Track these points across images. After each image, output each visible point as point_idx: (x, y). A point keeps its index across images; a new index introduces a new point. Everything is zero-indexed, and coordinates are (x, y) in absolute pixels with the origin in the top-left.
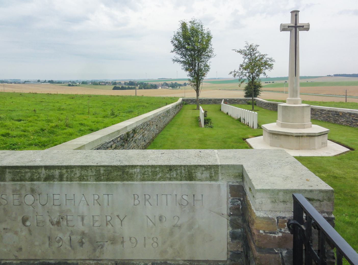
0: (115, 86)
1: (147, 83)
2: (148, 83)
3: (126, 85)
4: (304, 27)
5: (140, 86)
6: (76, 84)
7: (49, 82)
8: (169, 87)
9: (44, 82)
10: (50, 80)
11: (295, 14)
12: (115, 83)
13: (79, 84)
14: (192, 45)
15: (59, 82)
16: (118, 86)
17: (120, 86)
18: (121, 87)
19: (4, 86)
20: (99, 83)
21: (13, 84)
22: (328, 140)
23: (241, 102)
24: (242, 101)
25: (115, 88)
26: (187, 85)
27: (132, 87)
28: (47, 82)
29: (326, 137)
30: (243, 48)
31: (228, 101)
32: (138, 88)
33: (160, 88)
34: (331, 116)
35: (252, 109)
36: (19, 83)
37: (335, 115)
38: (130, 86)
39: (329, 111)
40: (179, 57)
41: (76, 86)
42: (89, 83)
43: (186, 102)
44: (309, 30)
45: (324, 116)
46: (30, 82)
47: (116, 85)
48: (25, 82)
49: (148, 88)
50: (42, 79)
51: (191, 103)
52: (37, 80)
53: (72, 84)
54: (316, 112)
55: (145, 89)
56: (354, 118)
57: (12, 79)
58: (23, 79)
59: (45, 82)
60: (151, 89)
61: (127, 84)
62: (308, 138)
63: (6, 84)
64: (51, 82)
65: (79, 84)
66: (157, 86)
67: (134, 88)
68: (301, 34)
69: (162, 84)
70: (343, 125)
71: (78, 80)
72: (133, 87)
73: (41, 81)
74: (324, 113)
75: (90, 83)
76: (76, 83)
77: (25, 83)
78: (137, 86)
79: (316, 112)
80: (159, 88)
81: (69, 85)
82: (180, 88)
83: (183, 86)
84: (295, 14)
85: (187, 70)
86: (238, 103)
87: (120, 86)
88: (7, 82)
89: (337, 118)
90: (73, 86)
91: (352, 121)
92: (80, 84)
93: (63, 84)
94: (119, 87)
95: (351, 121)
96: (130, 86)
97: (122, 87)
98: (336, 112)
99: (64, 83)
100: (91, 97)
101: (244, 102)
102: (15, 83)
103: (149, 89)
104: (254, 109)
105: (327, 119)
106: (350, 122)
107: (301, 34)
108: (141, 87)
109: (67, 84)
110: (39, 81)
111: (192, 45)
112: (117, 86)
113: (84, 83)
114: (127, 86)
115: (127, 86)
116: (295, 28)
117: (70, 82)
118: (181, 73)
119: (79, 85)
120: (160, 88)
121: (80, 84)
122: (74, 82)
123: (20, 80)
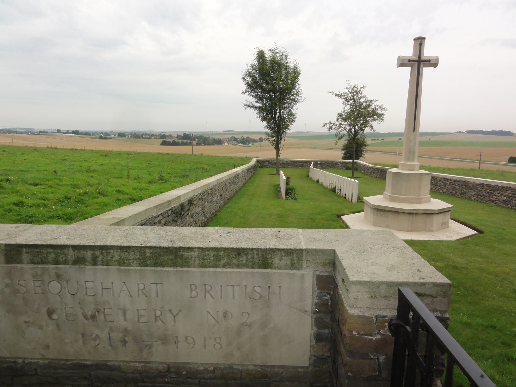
2: (209, 137)
4: (431, 62)
7: (73, 132)
8: (238, 143)
9: (66, 133)
10: (74, 129)
11: (420, 42)
14: (272, 84)
15: (87, 134)
17: (171, 141)
20: (142, 136)
21: (24, 135)
23: (336, 166)
25: (164, 143)
28: (70, 133)
31: (319, 164)
33: (226, 144)
34: (457, 187)
36: (32, 133)
38: (185, 141)
40: (253, 100)
41: (110, 138)
42: (128, 135)
43: (261, 164)
45: (449, 187)
46: (47, 132)
48: (41, 132)
50: (64, 128)
53: (104, 136)
56: (488, 191)
58: (37, 127)
59: (67, 132)
60: (213, 145)
62: (425, 216)
64: (76, 133)
72: (189, 141)
75: (130, 136)
76: (110, 135)
81: (101, 138)
84: (420, 42)
85: (263, 119)
87: (171, 141)
88: (16, 132)
90: (106, 138)
91: (485, 194)
93: (93, 136)
94: (169, 142)
96: (185, 141)
97: (173, 141)
98: (465, 182)
99: (93, 135)
100: (131, 154)
102: (27, 133)
106: (482, 196)
109: (98, 136)
110: (59, 131)
111: (272, 84)
112: (166, 140)
113: (121, 135)
114: (180, 141)
115: (180, 141)
116: (418, 63)
117: (102, 133)
120: (226, 144)
122: (106, 134)
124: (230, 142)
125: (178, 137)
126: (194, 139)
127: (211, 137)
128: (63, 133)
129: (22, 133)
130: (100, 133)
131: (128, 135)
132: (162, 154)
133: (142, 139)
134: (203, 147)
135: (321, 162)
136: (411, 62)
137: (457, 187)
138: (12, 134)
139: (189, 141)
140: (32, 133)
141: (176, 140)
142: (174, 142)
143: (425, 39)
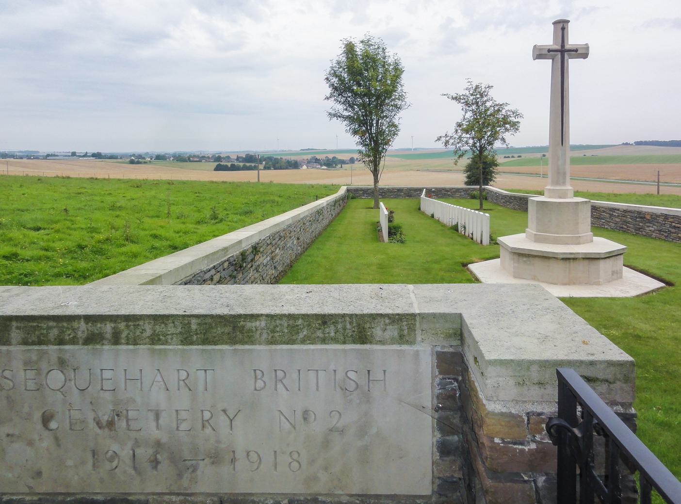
0: (218, 163)
1: (279, 157)
3: (240, 162)
6: (144, 160)
7: (94, 155)
8: (321, 166)
9: (84, 156)
10: (96, 152)
11: (561, 26)
12: (218, 159)
13: (149, 159)
14: (366, 86)
15: (112, 157)
16: (225, 164)
17: (229, 164)
18: (229, 166)
19: (7, 163)
20: (189, 159)
21: (25, 160)
23: (458, 195)
24: (460, 192)
26: (356, 162)
27: (251, 165)
28: (89, 156)
29: (620, 260)
30: (462, 92)
31: (434, 192)
32: (263, 168)
33: (305, 167)
34: (630, 220)
35: (479, 208)
36: (37, 158)
37: (638, 219)
38: (248, 164)
39: (625, 211)
40: (340, 108)
41: (145, 163)
42: (169, 158)
43: (353, 194)
45: (617, 220)
46: (57, 156)
47: (222, 162)
48: (48, 155)
49: (281, 168)
50: (80, 150)
51: (364, 195)
52: (69, 152)
53: (137, 160)
54: (602, 214)
55: (275, 169)
56: (674, 224)
58: (44, 150)
59: (86, 155)
60: (287, 168)
63: (12, 159)
64: (97, 156)
65: (149, 159)
66: (298, 164)
67: (255, 168)
68: (573, 64)
69: (307, 159)
71: (148, 151)
72: (253, 165)
73: (77, 154)
74: (617, 215)
75: (172, 158)
76: (144, 158)
77: (48, 158)
78: (261, 164)
79: (602, 214)
80: (302, 167)
81: (132, 162)
82: (341, 167)
83: (348, 163)
84: (561, 26)
85: (355, 132)
86: (452, 197)
87: (229, 164)
88: (13, 156)
89: (641, 224)
90: (139, 163)
91: (670, 229)
92: (151, 159)
95: (667, 230)
96: (248, 164)
97: (232, 165)
98: (639, 213)
99: (121, 158)
100: (173, 184)
101: (465, 194)
102: (29, 157)
103: (284, 169)
105: (621, 226)
106: (666, 232)
107: (573, 64)
108: (267, 166)
109: (128, 160)
110: (74, 154)
111: (366, 86)
112: (222, 163)
113: (159, 157)
114: (241, 164)
115: (241, 164)
116: (561, 53)
117: (134, 155)
119: (150, 161)
120: (305, 167)
121: (151, 159)
122: (140, 156)
123: (38, 152)
128: (80, 156)
133: (188, 163)
134: (273, 172)
137: (630, 220)
139: (253, 165)
143: (568, 22)
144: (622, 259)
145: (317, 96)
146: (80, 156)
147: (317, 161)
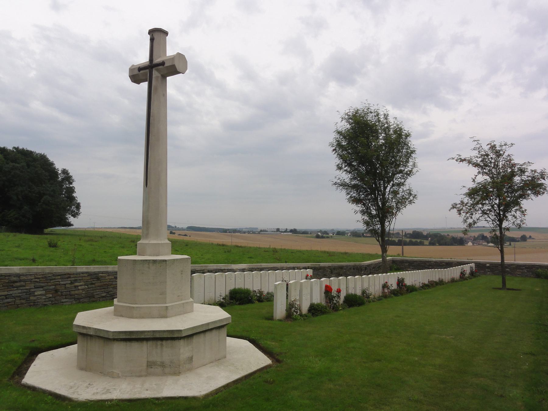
1: (446, 234)
2: (448, 235)
3: (408, 238)
4: (166, 65)
5: (431, 240)
7: (291, 231)
8: (488, 242)
9: (285, 232)
10: (292, 228)
11: (157, 35)
14: (372, 154)
15: (305, 232)
16: (393, 239)
17: (396, 240)
19: (232, 236)
20: (363, 234)
21: (246, 234)
22: (228, 336)
24: (522, 269)
26: (528, 240)
27: (417, 241)
28: (288, 232)
29: (224, 331)
31: (488, 267)
33: (470, 244)
35: (501, 287)
36: (254, 233)
38: (414, 240)
40: (346, 177)
41: (328, 237)
42: (348, 233)
43: (481, 268)
44: (139, 83)
48: (261, 231)
49: (446, 244)
50: (282, 227)
53: (322, 235)
57: (248, 227)
58: (261, 227)
59: (286, 231)
60: (452, 245)
61: (408, 236)
64: (294, 231)
67: (421, 244)
69: (474, 237)
70: (35, 304)
72: (419, 240)
75: (349, 234)
76: (328, 234)
78: (427, 240)
81: (318, 237)
82: (510, 245)
83: (518, 241)
84: (157, 35)
85: (356, 201)
87: (396, 240)
90: (322, 237)
93: (309, 235)
94: (394, 241)
96: (414, 240)
97: (399, 240)
99: (311, 234)
101: (528, 271)
102: (249, 232)
104: (508, 286)
110: (278, 230)
113: (340, 233)
114: (408, 240)
115: (408, 240)
116: (156, 71)
117: (321, 231)
118: (345, 214)
120: (470, 244)
122: (326, 232)
123: (257, 229)
124: (476, 242)
125: (406, 235)
126: (426, 237)
127: (451, 234)
128: (282, 232)
129: (245, 233)
130: (318, 232)
131: (348, 233)
132: (241, 247)
135: (491, 264)
136: (142, 72)
138: (237, 234)
139: (419, 240)
140: (254, 233)
141: (405, 239)
142: (411, 241)
144: (226, 331)
145: (330, 168)
146: (282, 232)
147: (484, 238)
